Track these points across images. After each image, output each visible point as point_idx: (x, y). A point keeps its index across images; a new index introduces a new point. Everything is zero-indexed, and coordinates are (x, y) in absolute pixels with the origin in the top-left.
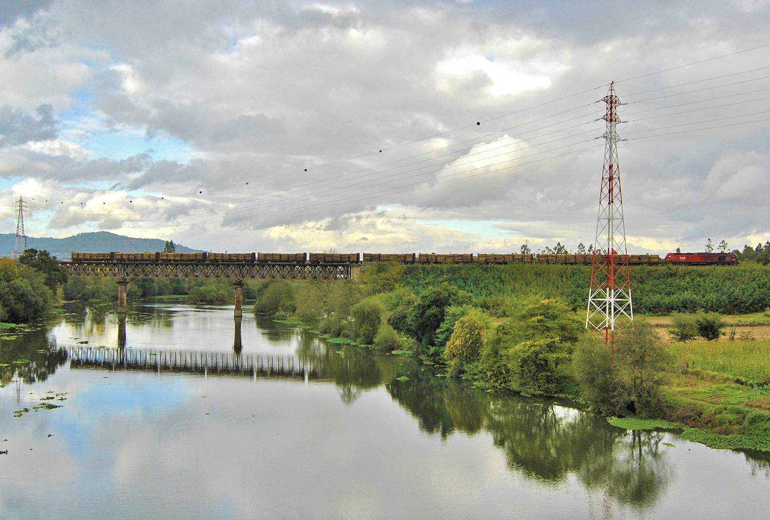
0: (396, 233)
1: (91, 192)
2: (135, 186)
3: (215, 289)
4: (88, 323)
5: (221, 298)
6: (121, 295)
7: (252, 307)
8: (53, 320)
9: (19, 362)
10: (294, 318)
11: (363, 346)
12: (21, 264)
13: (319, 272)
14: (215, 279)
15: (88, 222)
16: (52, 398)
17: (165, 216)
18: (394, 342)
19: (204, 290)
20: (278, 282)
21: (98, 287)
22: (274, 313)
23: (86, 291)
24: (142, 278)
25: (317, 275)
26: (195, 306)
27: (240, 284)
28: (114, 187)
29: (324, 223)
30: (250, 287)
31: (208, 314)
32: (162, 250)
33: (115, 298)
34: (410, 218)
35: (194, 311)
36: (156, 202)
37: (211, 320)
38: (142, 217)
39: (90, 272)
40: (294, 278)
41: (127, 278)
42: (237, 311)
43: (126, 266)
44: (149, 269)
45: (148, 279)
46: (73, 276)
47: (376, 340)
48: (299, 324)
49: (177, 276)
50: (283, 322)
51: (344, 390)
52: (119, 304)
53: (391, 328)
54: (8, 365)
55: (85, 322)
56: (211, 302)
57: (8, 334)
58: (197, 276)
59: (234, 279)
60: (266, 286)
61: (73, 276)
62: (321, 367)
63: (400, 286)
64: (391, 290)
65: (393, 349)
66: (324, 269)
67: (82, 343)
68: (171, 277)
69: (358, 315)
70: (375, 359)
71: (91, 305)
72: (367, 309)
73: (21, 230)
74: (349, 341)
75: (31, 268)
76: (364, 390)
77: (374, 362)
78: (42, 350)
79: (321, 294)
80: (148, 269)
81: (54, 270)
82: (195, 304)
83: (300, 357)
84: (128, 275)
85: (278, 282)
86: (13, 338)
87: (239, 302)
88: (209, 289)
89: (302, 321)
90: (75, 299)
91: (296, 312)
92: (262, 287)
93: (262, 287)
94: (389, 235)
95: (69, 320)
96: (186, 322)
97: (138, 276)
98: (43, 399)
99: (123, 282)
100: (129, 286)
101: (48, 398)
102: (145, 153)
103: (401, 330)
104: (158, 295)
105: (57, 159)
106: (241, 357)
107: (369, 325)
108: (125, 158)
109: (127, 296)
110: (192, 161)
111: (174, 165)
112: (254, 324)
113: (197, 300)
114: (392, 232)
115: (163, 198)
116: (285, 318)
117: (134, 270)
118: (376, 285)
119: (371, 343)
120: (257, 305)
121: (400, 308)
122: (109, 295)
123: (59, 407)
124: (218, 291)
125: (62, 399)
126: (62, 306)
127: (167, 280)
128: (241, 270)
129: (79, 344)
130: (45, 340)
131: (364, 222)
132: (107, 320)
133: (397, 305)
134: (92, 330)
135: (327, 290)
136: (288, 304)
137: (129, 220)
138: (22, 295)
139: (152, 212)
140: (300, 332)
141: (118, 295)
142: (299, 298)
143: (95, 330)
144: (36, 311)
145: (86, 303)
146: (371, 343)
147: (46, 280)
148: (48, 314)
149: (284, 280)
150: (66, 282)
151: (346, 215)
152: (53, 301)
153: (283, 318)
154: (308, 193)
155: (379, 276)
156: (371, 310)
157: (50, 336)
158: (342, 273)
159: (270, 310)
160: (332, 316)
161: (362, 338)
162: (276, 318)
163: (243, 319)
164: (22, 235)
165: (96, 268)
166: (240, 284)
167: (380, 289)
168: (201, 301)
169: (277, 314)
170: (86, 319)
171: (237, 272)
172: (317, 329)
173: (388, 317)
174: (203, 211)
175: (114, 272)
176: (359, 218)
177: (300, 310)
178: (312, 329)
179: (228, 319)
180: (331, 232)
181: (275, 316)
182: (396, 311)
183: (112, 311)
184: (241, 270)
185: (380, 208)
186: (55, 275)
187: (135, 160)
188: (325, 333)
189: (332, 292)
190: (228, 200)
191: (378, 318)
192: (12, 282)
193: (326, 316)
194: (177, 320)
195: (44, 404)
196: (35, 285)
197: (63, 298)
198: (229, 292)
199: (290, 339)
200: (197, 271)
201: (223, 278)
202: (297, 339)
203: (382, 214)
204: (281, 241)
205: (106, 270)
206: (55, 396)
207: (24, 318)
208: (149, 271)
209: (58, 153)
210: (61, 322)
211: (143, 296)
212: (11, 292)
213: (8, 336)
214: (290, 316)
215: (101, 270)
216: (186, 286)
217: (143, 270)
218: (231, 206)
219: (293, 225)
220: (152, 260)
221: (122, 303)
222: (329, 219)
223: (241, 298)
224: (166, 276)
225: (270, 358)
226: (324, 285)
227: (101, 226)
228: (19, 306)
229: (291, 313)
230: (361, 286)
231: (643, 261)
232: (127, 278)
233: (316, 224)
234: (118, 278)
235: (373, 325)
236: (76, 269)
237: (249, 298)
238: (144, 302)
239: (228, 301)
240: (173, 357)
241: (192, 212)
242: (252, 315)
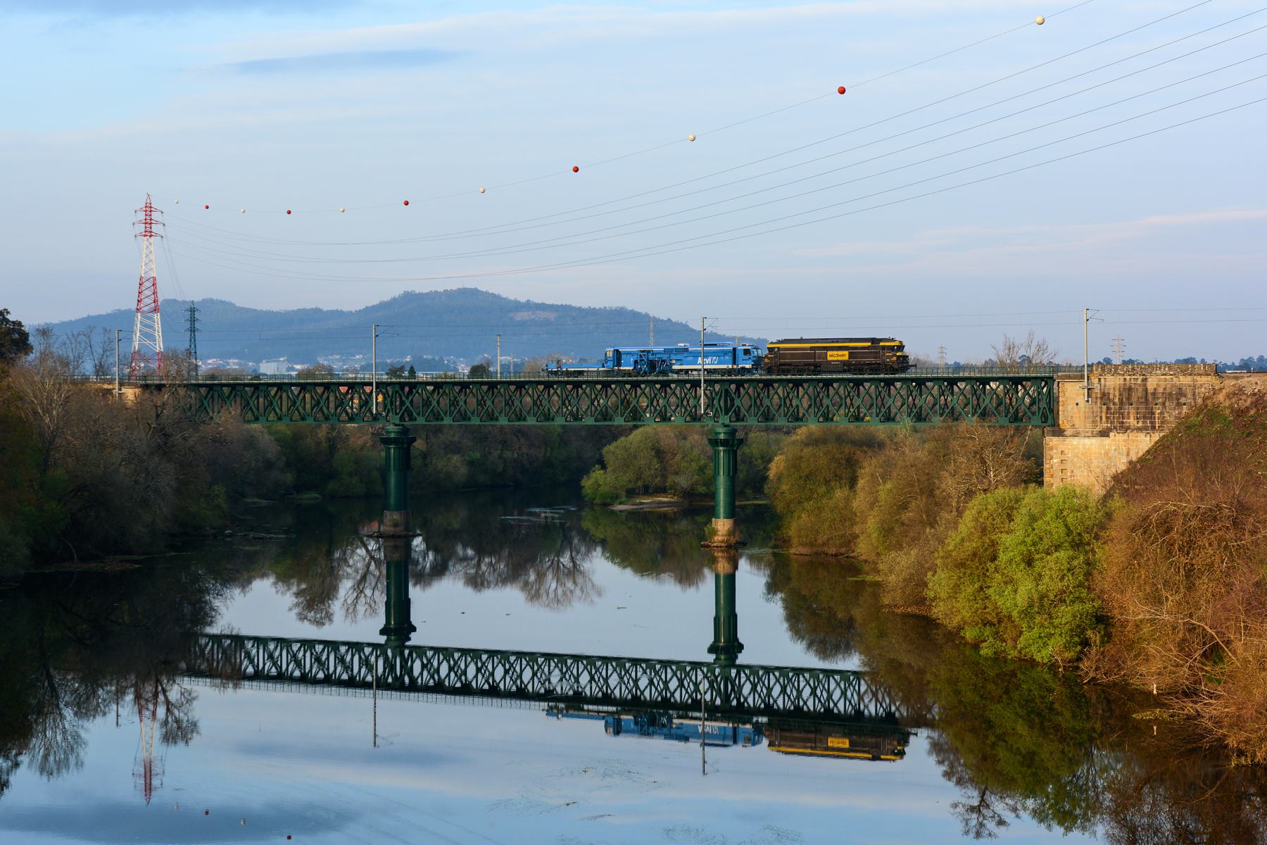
73: (148, 293)
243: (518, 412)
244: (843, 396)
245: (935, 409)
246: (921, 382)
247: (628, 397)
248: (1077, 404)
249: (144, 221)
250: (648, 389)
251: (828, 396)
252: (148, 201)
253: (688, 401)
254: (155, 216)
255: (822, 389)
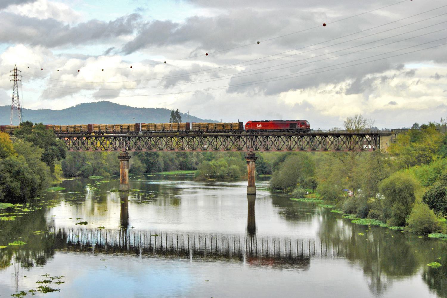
0: (432, 95)
1: (84, 58)
2: (130, 49)
3: (226, 163)
4: (89, 203)
5: (232, 174)
6: (123, 171)
7: (266, 184)
8: (52, 199)
9: (15, 244)
10: (314, 195)
11: (394, 228)
12: (17, 139)
13: (342, 143)
14: (226, 152)
15: (83, 92)
16: (49, 282)
17: (164, 83)
18: (431, 223)
19: (214, 164)
20: (296, 154)
21: (98, 163)
22: (292, 191)
23: (86, 167)
24: (146, 152)
25: (340, 145)
26: (204, 183)
27: (252, 157)
28: (108, 52)
29: (344, 85)
30: (265, 161)
31: (219, 192)
32: (166, 121)
33: (117, 175)
34: (443, 76)
35: (203, 188)
36: (154, 67)
37: (222, 197)
38: (138, 84)
39: (89, 146)
40: (314, 149)
41: (129, 152)
42: (250, 188)
43: (127, 138)
44: (153, 142)
45: (153, 154)
46: (72, 150)
47: (409, 221)
48: (320, 203)
49: (183, 149)
50: (302, 200)
51: (372, 279)
52: (121, 182)
53: (427, 207)
54: (4, 247)
55: (86, 201)
56: (221, 178)
57: (7, 214)
58: (205, 149)
59: (246, 151)
60: (282, 160)
61: (72, 150)
62: (346, 251)
63: (438, 158)
64: (428, 162)
65: (430, 232)
66: (348, 139)
67: (81, 223)
68: (176, 150)
69: (388, 192)
70: (409, 243)
71: (93, 182)
72: (398, 185)
73: (16, 102)
74: (377, 222)
75: (27, 142)
76: (396, 280)
77: (407, 248)
78: (39, 232)
79: (345, 168)
80: (152, 141)
81: (52, 144)
82: (204, 180)
83: (322, 242)
84: (130, 149)
85: (296, 154)
86: (12, 218)
87: (252, 178)
88: (219, 163)
89: (323, 199)
90: (75, 177)
91: (317, 189)
92: (278, 161)
93: (278, 161)
94: (423, 99)
95: (68, 199)
96: (195, 200)
97: (141, 149)
98: (40, 282)
99: (125, 157)
100: (131, 161)
101: (45, 282)
102: (134, 12)
103: (439, 209)
104: (164, 171)
105: (44, 23)
106: (255, 241)
107: (401, 204)
108: (113, 20)
109: (130, 172)
110: (190, 20)
111: (168, 25)
112: (270, 202)
113: (206, 176)
114: (426, 95)
115: (165, 62)
116: (305, 196)
117: (135, 143)
118: (409, 156)
119: (403, 224)
120: (272, 181)
121: (437, 184)
122: (111, 171)
123: (56, 291)
124: (229, 165)
125: (60, 283)
126: (60, 183)
127: (174, 154)
128: (254, 142)
129: (78, 225)
130: (43, 221)
131: (394, 82)
132: (109, 199)
133: (433, 180)
134: (93, 210)
135: (352, 164)
136: (307, 179)
137: (125, 88)
138: (18, 172)
139: (150, 79)
140: (321, 211)
141: (120, 171)
142: (320, 172)
143: (96, 210)
144: (33, 190)
145: (86, 180)
146: (403, 224)
147: (43, 156)
148: (45, 192)
149: (302, 152)
150: (64, 158)
151: (369, 76)
152: (51, 178)
153: (302, 196)
154: (327, 51)
155: (412, 147)
156: (403, 186)
157: (48, 217)
158: (369, 143)
159: (288, 187)
160: (358, 193)
161: (393, 219)
162: (294, 196)
163: (257, 197)
164: (17, 107)
165: (96, 141)
166: (252, 157)
167: (414, 162)
168: (211, 177)
169: (295, 191)
170: (87, 198)
171: (249, 143)
172: (340, 208)
173: (423, 194)
174: (206, 76)
175: (115, 146)
176: (384, 79)
177: (321, 187)
178: (335, 208)
179: (241, 196)
180: (354, 96)
181: (293, 193)
182: (433, 187)
183: (114, 189)
184: (254, 142)
185: (409, 67)
186: (52, 149)
187: (125, 21)
188: (350, 212)
189: (357, 165)
190: (235, 62)
191: (412, 195)
192: (7, 159)
193: (350, 194)
194: (184, 197)
195: (41, 287)
196: (31, 162)
197: (61, 175)
198: (240, 165)
199: (311, 220)
200: (205, 143)
201: (235, 151)
202: (319, 220)
203: (411, 73)
204: (298, 107)
205: (106, 144)
206: (51, 279)
207: (20, 197)
208: (152, 144)
209: (46, 16)
210: (337, 221)
211: (148, 171)
212: (6, 170)
213: (7, 216)
214: (310, 193)
215: (101, 144)
216: (194, 160)
217: (146, 143)
218: (240, 68)
219: (308, 89)
220: (132, 132)
221: (124, 180)
222: (349, 82)
223: (255, 173)
224: (171, 150)
225: (287, 242)
226: (348, 158)
227: (96, 96)
228: (16, 185)
229: (311, 190)
230: (392, 158)
231: (226, 129)
232: (129, 152)
233: (335, 87)
234: (120, 152)
235: (406, 204)
236: (74, 144)
237: (264, 174)
238: (149, 178)
239: (240, 176)
240: (180, 239)
241: (193, 77)
242: (267, 193)
243: (139, 147)
244: (210, 141)
245: (198, 147)
246: (314, 135)
247: (148, 141)
248: (387, 144)
249: (14, 75)
250: (210, 138)
251: (267, 140)
252: (16, 67)
253: (169, 143)
254: (18, 73)
255: (277, 138)
